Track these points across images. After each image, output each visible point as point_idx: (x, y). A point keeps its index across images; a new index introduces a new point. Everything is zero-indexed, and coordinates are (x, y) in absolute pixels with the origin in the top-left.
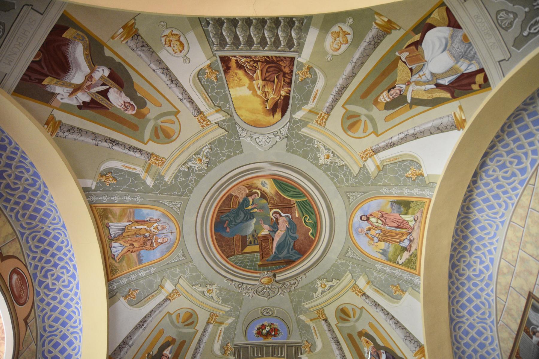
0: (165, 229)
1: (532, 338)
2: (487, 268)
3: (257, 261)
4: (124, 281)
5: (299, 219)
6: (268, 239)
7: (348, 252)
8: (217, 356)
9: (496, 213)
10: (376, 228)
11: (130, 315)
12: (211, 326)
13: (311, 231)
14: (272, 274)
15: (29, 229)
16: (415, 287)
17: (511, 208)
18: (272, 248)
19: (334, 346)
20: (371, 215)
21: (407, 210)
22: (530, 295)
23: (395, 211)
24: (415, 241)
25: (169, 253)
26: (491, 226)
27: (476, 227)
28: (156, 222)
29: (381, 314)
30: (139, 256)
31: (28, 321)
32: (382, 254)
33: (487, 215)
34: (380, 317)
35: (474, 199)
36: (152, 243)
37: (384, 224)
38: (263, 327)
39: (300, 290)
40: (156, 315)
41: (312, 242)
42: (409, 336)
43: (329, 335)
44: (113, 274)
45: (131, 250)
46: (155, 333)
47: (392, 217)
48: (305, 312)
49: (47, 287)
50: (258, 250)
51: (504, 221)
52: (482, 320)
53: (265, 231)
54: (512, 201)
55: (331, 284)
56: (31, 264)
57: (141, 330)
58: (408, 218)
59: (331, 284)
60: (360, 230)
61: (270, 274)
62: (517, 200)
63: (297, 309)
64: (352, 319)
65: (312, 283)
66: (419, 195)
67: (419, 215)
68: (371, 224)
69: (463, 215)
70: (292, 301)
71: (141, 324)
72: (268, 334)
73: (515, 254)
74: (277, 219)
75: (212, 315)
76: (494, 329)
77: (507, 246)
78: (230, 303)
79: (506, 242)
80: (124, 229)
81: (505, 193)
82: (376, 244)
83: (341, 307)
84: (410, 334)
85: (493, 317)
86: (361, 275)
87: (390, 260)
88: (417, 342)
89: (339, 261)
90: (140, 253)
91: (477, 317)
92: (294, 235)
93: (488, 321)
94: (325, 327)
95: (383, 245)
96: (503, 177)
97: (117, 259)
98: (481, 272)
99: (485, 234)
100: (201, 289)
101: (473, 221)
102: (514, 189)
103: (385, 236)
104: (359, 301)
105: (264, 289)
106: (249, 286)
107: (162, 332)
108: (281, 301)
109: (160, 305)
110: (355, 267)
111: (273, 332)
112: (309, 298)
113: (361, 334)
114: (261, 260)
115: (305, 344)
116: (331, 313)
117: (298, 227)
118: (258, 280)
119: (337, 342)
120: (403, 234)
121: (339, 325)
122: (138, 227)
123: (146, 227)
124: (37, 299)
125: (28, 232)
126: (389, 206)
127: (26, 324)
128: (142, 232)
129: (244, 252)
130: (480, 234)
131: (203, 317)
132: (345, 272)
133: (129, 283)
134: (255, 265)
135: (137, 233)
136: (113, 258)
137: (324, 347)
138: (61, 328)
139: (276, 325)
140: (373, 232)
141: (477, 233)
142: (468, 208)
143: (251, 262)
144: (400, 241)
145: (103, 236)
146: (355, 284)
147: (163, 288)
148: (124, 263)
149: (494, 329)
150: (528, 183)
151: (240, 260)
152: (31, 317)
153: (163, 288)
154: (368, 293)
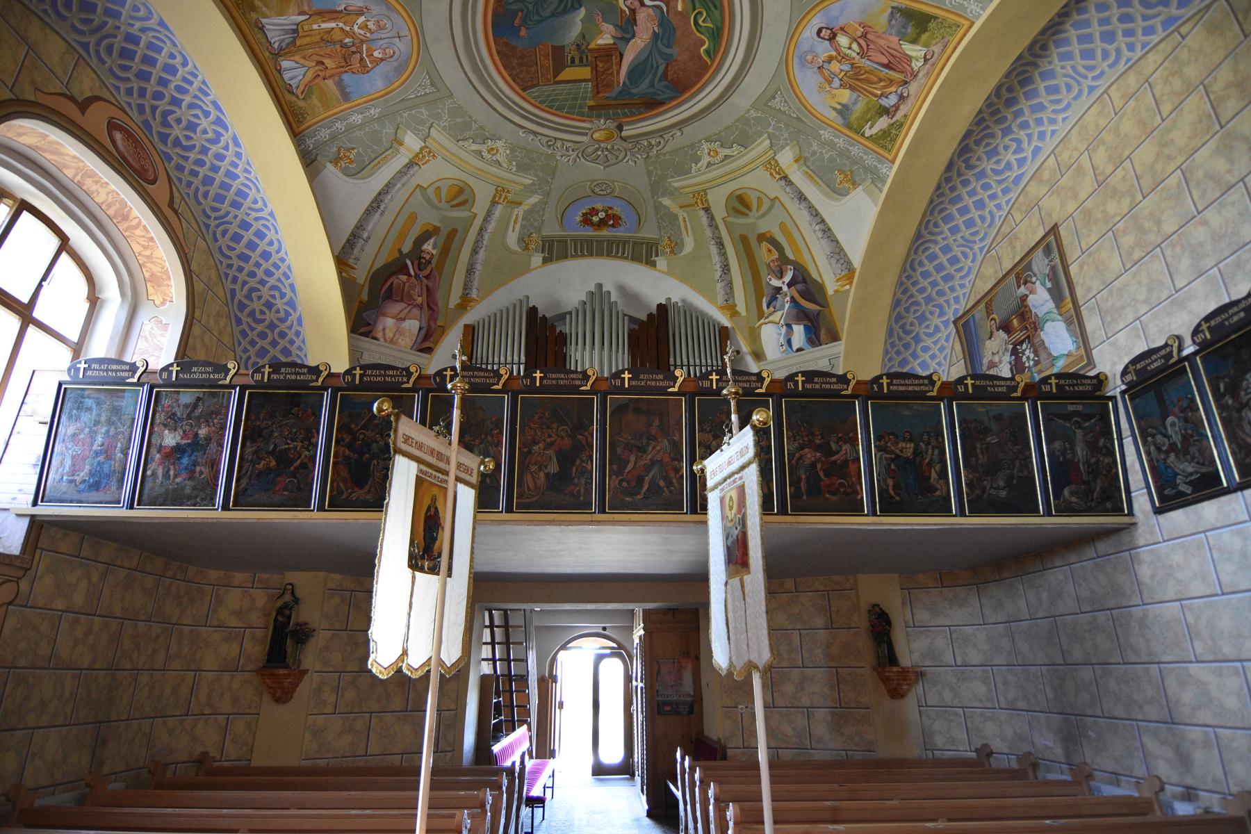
0: (383, 28)
1: (1019, 287)
2: (1021, 162)
3: (585, 99)
4: (324, 134)
5: (684, 15)
6: (610, 55)
7: (774, 98)
8: (514, 253)
9: (1090, 68)
10: (843, 58)
11: (355, 195)
12: (499, 208)
13: (706, 46)
14: (615, 124)
15: (92, 32)
16: (878, 179)
17: (1121, 67)
18: (618, 73)
19: (714, 250)
20: (842, 29)
21: (919, 35)
22: (1054, 230)
23: (893, 31)
24: (909, 101)
25: (403, 79)
26: (965, 255)
27: (1041, 86)
28: (362, 14)
29: (805, 213)
30: (340, 85)
31: (176, 207)
32: (839, 112)
33: (1073, 68)
34: (802, 217)
35: (1065, 32)
36: (362, 59)
37: (862, 54)
38: (594, 211)
39: (667, 157)
40: (399, 189)
41: (704, 68)
42: (838, 253)
43: (708, 233)
44: (300, 123)
45: (322, 74)
46: (401, 221)
47: (882, 42)
48: (672, 193)
49: (177, 143)
50: (589, 77)
51: (1095, 87)
52: (968, 243)
53: (605, 39)
54: (1131, 54)
55: (728, 152)
56: (129, 104)
57: (377, 215)
58: (915, 51)
59: (728, 152)
60: (809, 57)
61: (612, 125)
62: (1139, 54)
63: (658, 187)
64: (754, 213)
65: (692, 146)
66: (954, 7)
67: (937, 49)
68: (836, 50)
69: (1028, 58)
70: (649, 173)
71: (375, 205)
72: (602, 223)
73: (1076, 155)
74: (633, 12)
75: (500, 191)
76: (980, 258)
77: (1074, 137)
78: (532, 172)
79: (1076, 128)
80: (295, 31)
81: (1129, 33)
82: (834, 91)
83: (738, 193)
84: (842, 250)
85: (988, 241)
86: (787, 145)
87: (849, 126)
88: (849, 263)
89: (753, 114)
90: (341, 80)
91: (963, 238)
92: (668, 51)
93: (976, 247)
94: (704, 220)
95: (845, 96)
96: (926, 334)
97: (299, 92)
98: (1009, 166)
99: (1053, 102)
100: (475, 147)
101: (1040, 74)
102: (1149, 31)
103: (856, 79)
104: (773, 188)
105: (597, 150)
106: (569, 144)
107: (413, 217)
108: (629, 173)
109: (402, 173)
110: (780, 129)
111: (612, 220)
112: (683, 171)
113: (762, 238)
114: (594, 97)
115: (666, 241)
116: (718, 200)
117: (678, 34)
118: (586, 134)
119: (720, 244)
120: (891, 82)
121: (730, 219)
122: (324, 26)
123: (341, 25)
124: (171, 167)
125: (93, 40)
126: (884, 18)
127: (176, 212)
128: (337, 36)
129: (558, 79)
130: (1043, 99)
131: (483, 194)
132: (760, 135)
133: (334, 137)
134: (581, 106)
135: (326, 39)
136: (291, 92)
137: (695, 249)
138: (234, 211)
139: (618, 210)
140: (835, 66)
141: (1038, 96)
142: (1044, 47)
143: (573, 99)
144: (882, 95)
145: (256, 48)
146: (773, 158)
147: (401, 144)
148: (315, 100)
149: (980, 258)
150: (1177, 30)
151: (549, 95)
152: (177, 200)
153: (401, 144)
154: (793, 177)
